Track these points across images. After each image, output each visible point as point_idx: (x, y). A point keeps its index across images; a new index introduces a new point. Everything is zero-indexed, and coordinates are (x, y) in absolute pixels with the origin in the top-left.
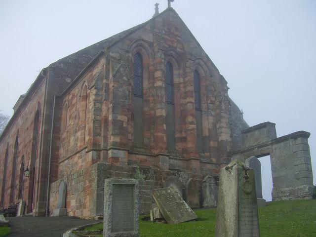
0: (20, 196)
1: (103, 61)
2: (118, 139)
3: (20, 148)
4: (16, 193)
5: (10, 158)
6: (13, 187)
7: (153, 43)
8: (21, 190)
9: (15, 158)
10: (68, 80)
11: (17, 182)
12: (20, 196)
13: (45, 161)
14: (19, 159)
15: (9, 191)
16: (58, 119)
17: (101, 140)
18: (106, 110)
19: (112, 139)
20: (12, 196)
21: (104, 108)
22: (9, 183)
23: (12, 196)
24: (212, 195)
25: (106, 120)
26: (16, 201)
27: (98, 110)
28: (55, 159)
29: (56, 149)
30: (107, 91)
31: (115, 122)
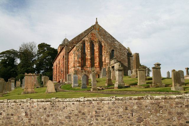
0: (61, 78)
1: (75, 47)
2: (79, 65)
3: (60, 65)
4: (60, 77)
5: (58, 67)
6: (59, 76)
7: (87, 40)
8: (61, 76)
9: (59, 67)
10: (70, 48)
11: (60, 74)
12: (61, 78)
13: (66, 69)
14: (60, 68)
15: (58, 77)
16: (68, 58)
17: (75, 65)
18: (76, 58)
19: (77, 65)
20: (59, 79)
21: (76, 58)
22: (58, 75)
23: (59, 79)
24: (175, 118)
25: (76, 61)
26: (60, 80)
27: (74, 59)
28: (68, 68)
29: (68, 66)
30: (76, 54)
31: (78, 61)
